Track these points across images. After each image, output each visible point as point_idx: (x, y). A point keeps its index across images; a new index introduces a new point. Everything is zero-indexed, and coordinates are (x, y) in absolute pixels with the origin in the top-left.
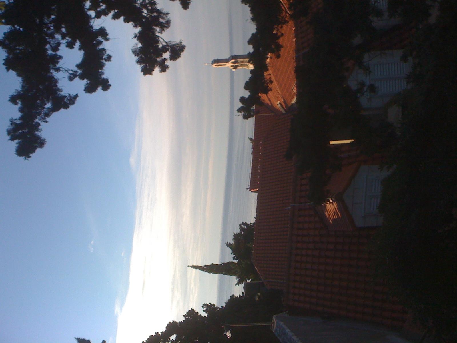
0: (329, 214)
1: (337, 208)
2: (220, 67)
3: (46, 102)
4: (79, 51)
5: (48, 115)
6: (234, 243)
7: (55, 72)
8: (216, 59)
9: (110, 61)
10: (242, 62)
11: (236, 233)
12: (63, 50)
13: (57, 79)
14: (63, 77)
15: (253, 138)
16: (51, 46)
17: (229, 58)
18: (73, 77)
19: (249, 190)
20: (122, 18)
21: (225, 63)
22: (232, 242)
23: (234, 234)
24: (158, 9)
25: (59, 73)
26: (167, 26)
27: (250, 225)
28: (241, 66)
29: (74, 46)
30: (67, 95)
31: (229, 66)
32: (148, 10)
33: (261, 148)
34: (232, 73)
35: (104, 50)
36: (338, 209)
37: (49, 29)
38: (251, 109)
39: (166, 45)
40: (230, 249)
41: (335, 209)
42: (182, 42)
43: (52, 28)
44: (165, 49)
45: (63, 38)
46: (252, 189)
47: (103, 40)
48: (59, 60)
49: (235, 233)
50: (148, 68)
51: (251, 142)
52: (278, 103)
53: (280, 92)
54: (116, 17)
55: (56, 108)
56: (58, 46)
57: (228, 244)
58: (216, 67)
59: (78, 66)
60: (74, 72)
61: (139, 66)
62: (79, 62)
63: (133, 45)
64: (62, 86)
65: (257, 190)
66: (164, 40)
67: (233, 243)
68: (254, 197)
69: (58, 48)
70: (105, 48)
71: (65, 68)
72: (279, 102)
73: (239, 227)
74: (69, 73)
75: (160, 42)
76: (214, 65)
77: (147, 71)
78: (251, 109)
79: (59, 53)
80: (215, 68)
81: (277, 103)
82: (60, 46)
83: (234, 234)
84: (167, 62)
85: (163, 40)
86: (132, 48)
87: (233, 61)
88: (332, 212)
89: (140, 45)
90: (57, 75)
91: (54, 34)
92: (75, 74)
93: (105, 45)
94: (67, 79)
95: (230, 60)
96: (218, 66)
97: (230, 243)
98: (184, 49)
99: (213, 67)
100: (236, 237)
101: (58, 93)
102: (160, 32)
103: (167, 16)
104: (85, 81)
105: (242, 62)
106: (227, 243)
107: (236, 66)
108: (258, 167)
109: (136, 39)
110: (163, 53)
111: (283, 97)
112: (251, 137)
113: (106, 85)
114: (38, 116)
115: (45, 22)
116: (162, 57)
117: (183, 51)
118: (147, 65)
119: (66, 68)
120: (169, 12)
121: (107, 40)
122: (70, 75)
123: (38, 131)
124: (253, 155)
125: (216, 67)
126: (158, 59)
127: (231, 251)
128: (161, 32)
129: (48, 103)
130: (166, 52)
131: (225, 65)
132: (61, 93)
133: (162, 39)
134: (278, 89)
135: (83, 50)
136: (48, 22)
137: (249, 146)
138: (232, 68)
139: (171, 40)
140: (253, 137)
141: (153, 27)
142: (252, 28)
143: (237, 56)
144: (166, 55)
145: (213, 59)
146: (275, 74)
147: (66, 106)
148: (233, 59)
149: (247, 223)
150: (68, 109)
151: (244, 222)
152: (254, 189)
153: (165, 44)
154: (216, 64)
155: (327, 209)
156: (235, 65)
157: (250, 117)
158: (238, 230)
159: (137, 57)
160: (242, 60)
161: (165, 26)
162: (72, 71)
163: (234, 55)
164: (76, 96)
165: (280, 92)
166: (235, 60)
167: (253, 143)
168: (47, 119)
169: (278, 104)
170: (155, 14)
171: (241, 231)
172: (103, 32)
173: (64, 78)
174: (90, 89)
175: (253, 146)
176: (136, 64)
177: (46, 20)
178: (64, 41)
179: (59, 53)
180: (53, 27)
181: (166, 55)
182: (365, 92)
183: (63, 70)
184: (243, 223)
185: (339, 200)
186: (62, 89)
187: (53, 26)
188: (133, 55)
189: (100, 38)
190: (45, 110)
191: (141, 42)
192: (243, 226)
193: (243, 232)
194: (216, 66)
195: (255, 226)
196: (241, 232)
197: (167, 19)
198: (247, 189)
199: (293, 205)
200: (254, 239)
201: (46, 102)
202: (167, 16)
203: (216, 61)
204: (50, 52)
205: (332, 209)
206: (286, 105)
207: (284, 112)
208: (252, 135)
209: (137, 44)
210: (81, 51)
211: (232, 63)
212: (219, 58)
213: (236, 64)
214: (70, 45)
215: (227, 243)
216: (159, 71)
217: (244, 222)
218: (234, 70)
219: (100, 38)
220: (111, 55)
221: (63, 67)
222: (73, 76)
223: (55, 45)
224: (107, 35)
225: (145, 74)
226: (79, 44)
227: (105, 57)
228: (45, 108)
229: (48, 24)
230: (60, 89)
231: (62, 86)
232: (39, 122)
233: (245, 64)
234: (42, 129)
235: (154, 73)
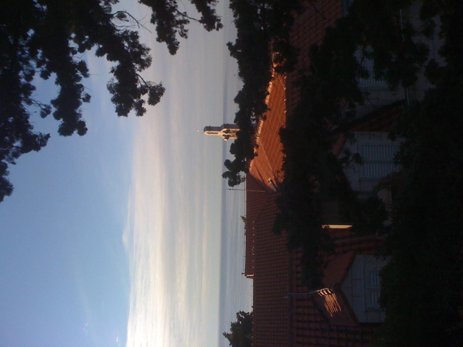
0: (328, 307)
2: (211, 135)
3: (16, 140)
4: (56, 85)
5: (16, 155)
6: (232, 333)
7: (27, 104)
8: (208, 126)
9: (89, 102)
11: (234, 323)
12: (37, 80)
13: (28, 113)
14: (34, 111)
15: (246, 217)
16: (24, 73)
17: (221, 126)
18: (46, 113)
19: (244, 275)
20: (106, 56)
22: (230, 332)
23: (232, 323)
24: (140, 43)
25: (31, 106)
26: (147, 64)
27: (247, 314)
29: (49, 77)
30: (38, 134)
31: (221, 135)
32: (129, 43)
33: (254, 228)
34: (224, 142)
35: (81, 86)
37: (23, 53)
38: (237, 175)
39: (145, 86)
40: (228, 339)
42: (162, 84)
43: (27, 52)
44: (143, 90)
45: (39, 66)
46: (248, 275)
47: (82, 76)
48: (32, 91)
49: (233, 323)
50: (123, 108)
51: (244, 222)
52: (269, 180)
53: (271, 169)
54: (100, 53)
55: (25, 149)
56: (32, 75)
57: (226, 334)
58: (208, 135)
59: (53, 102)
60: (47, 108)
61: (114, 105)
62: (55, 98)
63: (109, 80)
64: (33, 122)
65: (253, 275)
66: (144, 79)
67: (231, 334)
68: (250, 282)
69: (32, 77)
70: (83, 84)
71: (38, 101)
72: (270, 178)
73: (236, 317)
74: (41, 108)
75: (138, 81)
76: (206, 133)
77: (122, 111)
78: (237, 175)
79: (32, 83)
81: (268, 180)
82: (34, 75)
83: (232, 323)
84: (145, 105)
85: (142, 79)
86: (107, 83)
87: (225, 130)
89: (116, 81)
90: (29, 109)
91: (29, 59)
92: (48, 109)
93: (84, 81)
94: (39, 115)
95: (223, 129)
96: (210, 133)
97: (228, 333)
98: (164, 92)
99: (205, 134)
100: (234, 326)
101: (29, 130)
102: (139, 69)
103: (148, 52)
104: (61, 121)
106: (225, 333)
107: (227, 135)
108: (252, 250)
109: (113, 74)
110: (141, 95)
111: (273, 173)
112: (244, 216)
113: (82, 129)
114: (6, 156)
115: (20, 44)
116: (140, 98)
117: (162, 94)
118: (122, 104)
119: (39, 101)
120: (150, 48)
121: (86, 76)
122: (43, 111)
123: (6, 175)
124: (246, 236)
125: (208, 134)
126: (135, 100)
127: (229, 343)
128: (140, 70)
129: (18, 140)
130: (145, 94)
131: (217, 133)
132: (31, 130)
133: (141, 78)
134: (269, 165)
135: (60, 84)
136: (24, 44)
137: (242, 225)
138: (224, 137)
139: (150, 81)
140: (245, 216)
141: (134, 64)
143: (229, 125)
144: (145, 97)
145: (205, 126)
146: (266, 148)
147: (37, 148)
148: (225, 128)
149: (245, 312)
150: (39, 151)
151: (242, 311)
152: (249, 275)
153: (144, 84)
154: (208, 132)
157: (236, 184)
158: (235, 320)
159: (112, 94)
161: (145, 64)
162: (45, 105)
163: (226, 123)
164: (48, 136)
165: (271, 169)
166: (227, 130)
167: (246, 222)
168: (15, 160)
169: (269, 181)
170: (137, 50)
171: (239, 321)
172: (83, 67)
173: (36, 112)
174: (65, 131)
175: (246, 226)
176: (111, 102)
177: (21, 42)
178: (39, 70)
179: (32, 83)
180: (28, 51)
181: (145, 97)
182: (351, 161)
183: (35, 103)
184: (240, 312)
186: (33, 126)
187: (29, 50)
188: (108, 92)
189: (79, 73)
190: (14, 148)
191: (118, 78)
192: (240, 315)
193: (240, 322)
194: (207, 133)
195: (253, 316)
196: (239, 322)
197: (148, 55)
198: (242, 274)
200: (253, 330)
201: (16, 140)
202: (148, 52)
203: (209, 129)
204: (23, 80)
206: (277, 182)
207: (275, 190)
208: (244, 214)
209: (113, 80)
210: (58, 85)
211: (224, 132)
212: (212, 126)
213: (228, 134)
214: (45, 75)
215: (224, 333)
216: (136, 114)
217: (242, 311)
218: (226, 140)
219: (79, 73)
220: (90, 95)
221: (36, 100)
222: (46, 112)
223: (29, 73)
224: (87, 70)
225: (120, 115)
226: (56, 77)
227: (83, 96)
228: (13, 146)
229: (24, 46)
230: (31, 126)
231: (33, 122)
232: (7, 162)
234: (9, 172)
235: (129, 114)
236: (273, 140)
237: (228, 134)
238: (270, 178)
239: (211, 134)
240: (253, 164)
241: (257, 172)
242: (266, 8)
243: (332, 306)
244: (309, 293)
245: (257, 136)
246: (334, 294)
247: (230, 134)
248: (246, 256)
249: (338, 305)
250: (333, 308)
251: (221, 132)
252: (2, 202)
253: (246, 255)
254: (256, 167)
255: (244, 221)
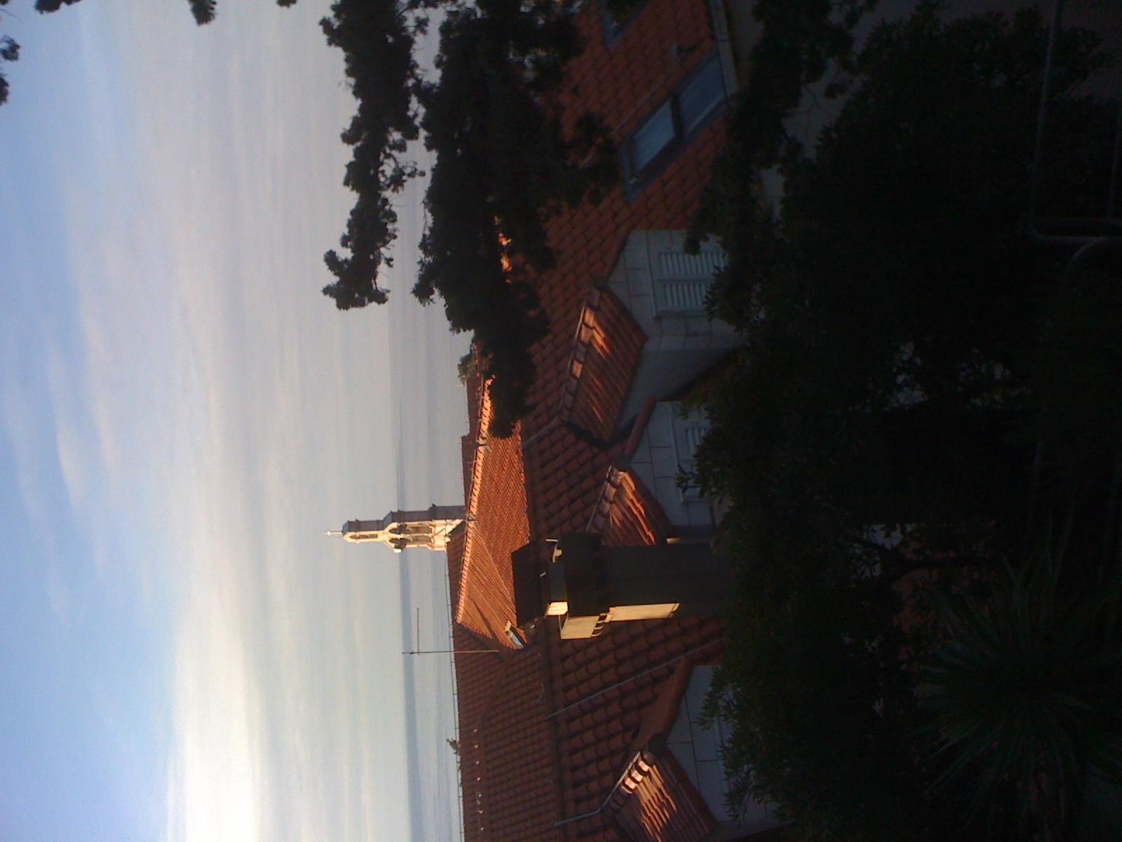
0: (649, 818)
1: (663, 785)
2: (363, 543)
8: (353, 520)
10: (417, 529)
17: (385, 518)
21: (374, 530)
28: (416, 540)
36: (665, 788)
41: (660, 790)
52: (508, 628)
72: (509, 624)
80: (351, 543)
87: (394, 525)
88: (656, 807)
95: (388, 524)
96: (359, 538)
105: (417, 529)
124: (462, 773)
125: (354, 540)
131: (376, 536)
137: (452, 760)
138: (393, 545)
142: (350, 107)
148: (393, 521)
150: (9, 97)
154: (352, 534)
155: (643, 805)
156: (399, 537)
160: (415, 524)
166: (399, 525)
169: (507, 633)
185: (662, 757)
194: (352, 537)
199: (561, 823)
203: (354, 526)
205: (653, 797)
211: (392, 531)
233: (424, 536)
236: (505, 519)
237: (402, 536)
238: (509, 624)
239: (362, 540)
240: (467, 598)
241: (478, 615)
242: (508, 283)
243: (656, 810)
244: (600, 809)
245: (469, 520)
246: (654, 767)
247: (407, 536)
248: (463, 797)
249: (667, 796)
250: (659, 815)
251: (384, 533)
252: (4, 106)
253: (465, 827)
254: (475, 603)
255: (455, 751)
